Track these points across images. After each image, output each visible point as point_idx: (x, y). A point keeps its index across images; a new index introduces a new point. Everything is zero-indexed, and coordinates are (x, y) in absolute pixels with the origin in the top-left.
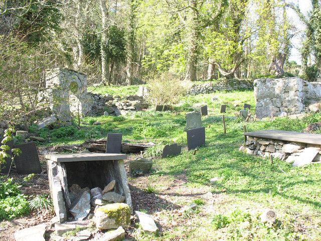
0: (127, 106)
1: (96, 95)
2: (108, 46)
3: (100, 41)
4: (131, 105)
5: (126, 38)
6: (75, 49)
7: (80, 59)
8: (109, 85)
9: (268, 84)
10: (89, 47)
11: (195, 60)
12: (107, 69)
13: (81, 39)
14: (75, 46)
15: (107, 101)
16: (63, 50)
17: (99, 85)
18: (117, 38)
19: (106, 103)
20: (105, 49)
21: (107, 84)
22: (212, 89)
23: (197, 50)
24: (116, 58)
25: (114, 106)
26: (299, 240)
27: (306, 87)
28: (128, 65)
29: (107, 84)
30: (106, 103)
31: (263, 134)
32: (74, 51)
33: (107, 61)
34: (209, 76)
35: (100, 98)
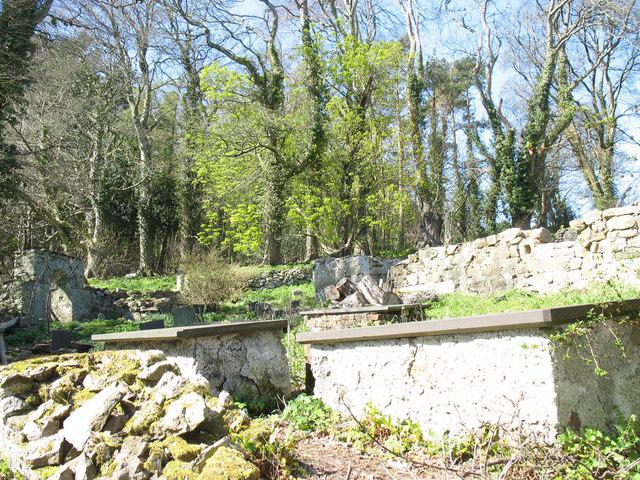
0: (147, 306)
1: (99, 289)
2: (151, 208)
3: (138, 199)
4: (153, 305)
5: (179, 194)
6: (88, 215)
7: (96, 231)
8: (152, 275)
9: (328, 265)
10: (120, 211)
11: (278, 231)
12: (149, 249)
13: (98, 198)
14: (90, 210)
15: (116, 299)
16: (58, 219)
17: (134, 275)
18: (164, 191)
19: (115, 303)
20: (144, 214)
21: (148, 273)
22: (304, 278)
23: (279, 214)
24: (163, 227)
25: (126, 307)
26: (567, 477)
27: (378, 269)
28: (183, 242)
29: (148, 273)
30: (115, 303)
31: (169, 336)
32: (87, 218)
33: (151, 234)
34: (308, 254)
35: (105, 295)
